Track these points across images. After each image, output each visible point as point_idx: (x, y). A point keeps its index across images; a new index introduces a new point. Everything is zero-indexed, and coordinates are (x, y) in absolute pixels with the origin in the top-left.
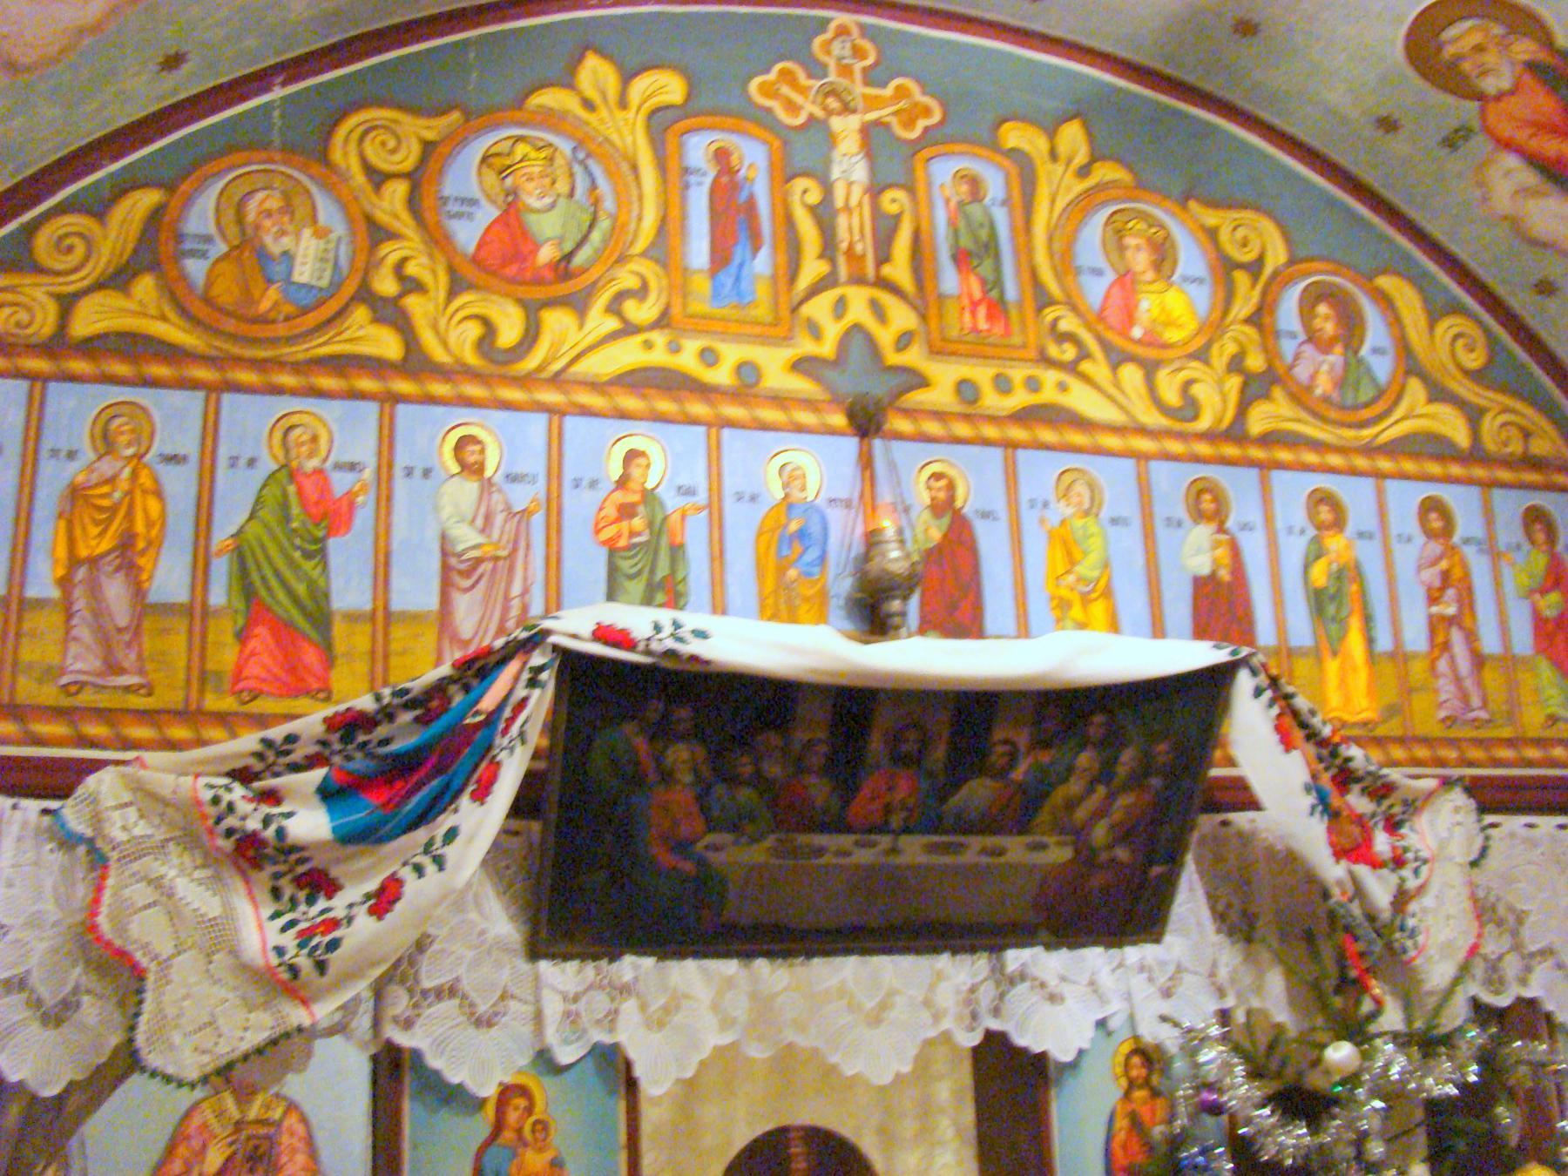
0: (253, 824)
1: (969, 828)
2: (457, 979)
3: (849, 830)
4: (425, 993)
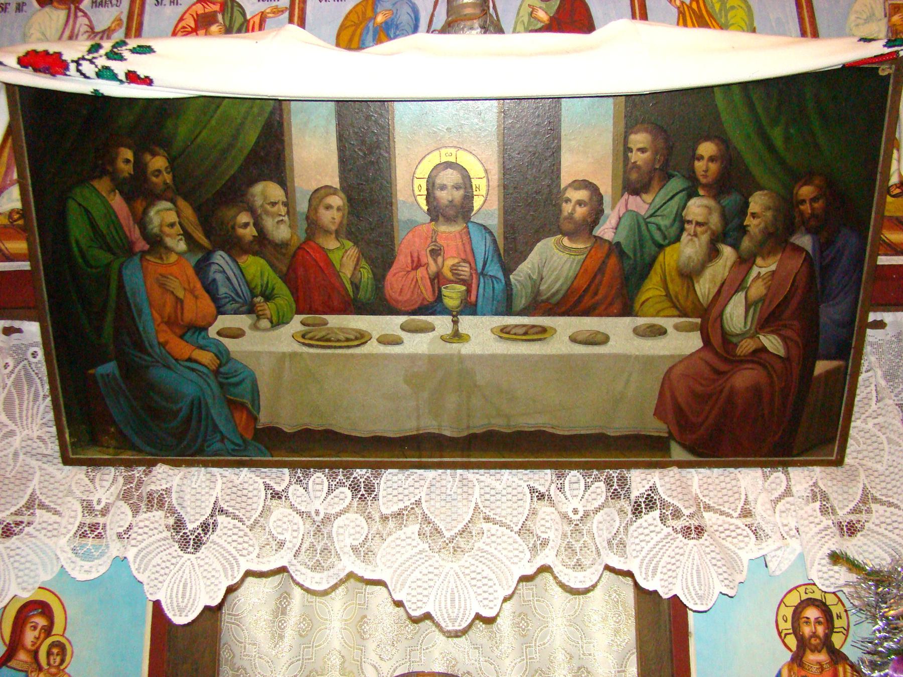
2: (168, 491)
4: (385, 518)
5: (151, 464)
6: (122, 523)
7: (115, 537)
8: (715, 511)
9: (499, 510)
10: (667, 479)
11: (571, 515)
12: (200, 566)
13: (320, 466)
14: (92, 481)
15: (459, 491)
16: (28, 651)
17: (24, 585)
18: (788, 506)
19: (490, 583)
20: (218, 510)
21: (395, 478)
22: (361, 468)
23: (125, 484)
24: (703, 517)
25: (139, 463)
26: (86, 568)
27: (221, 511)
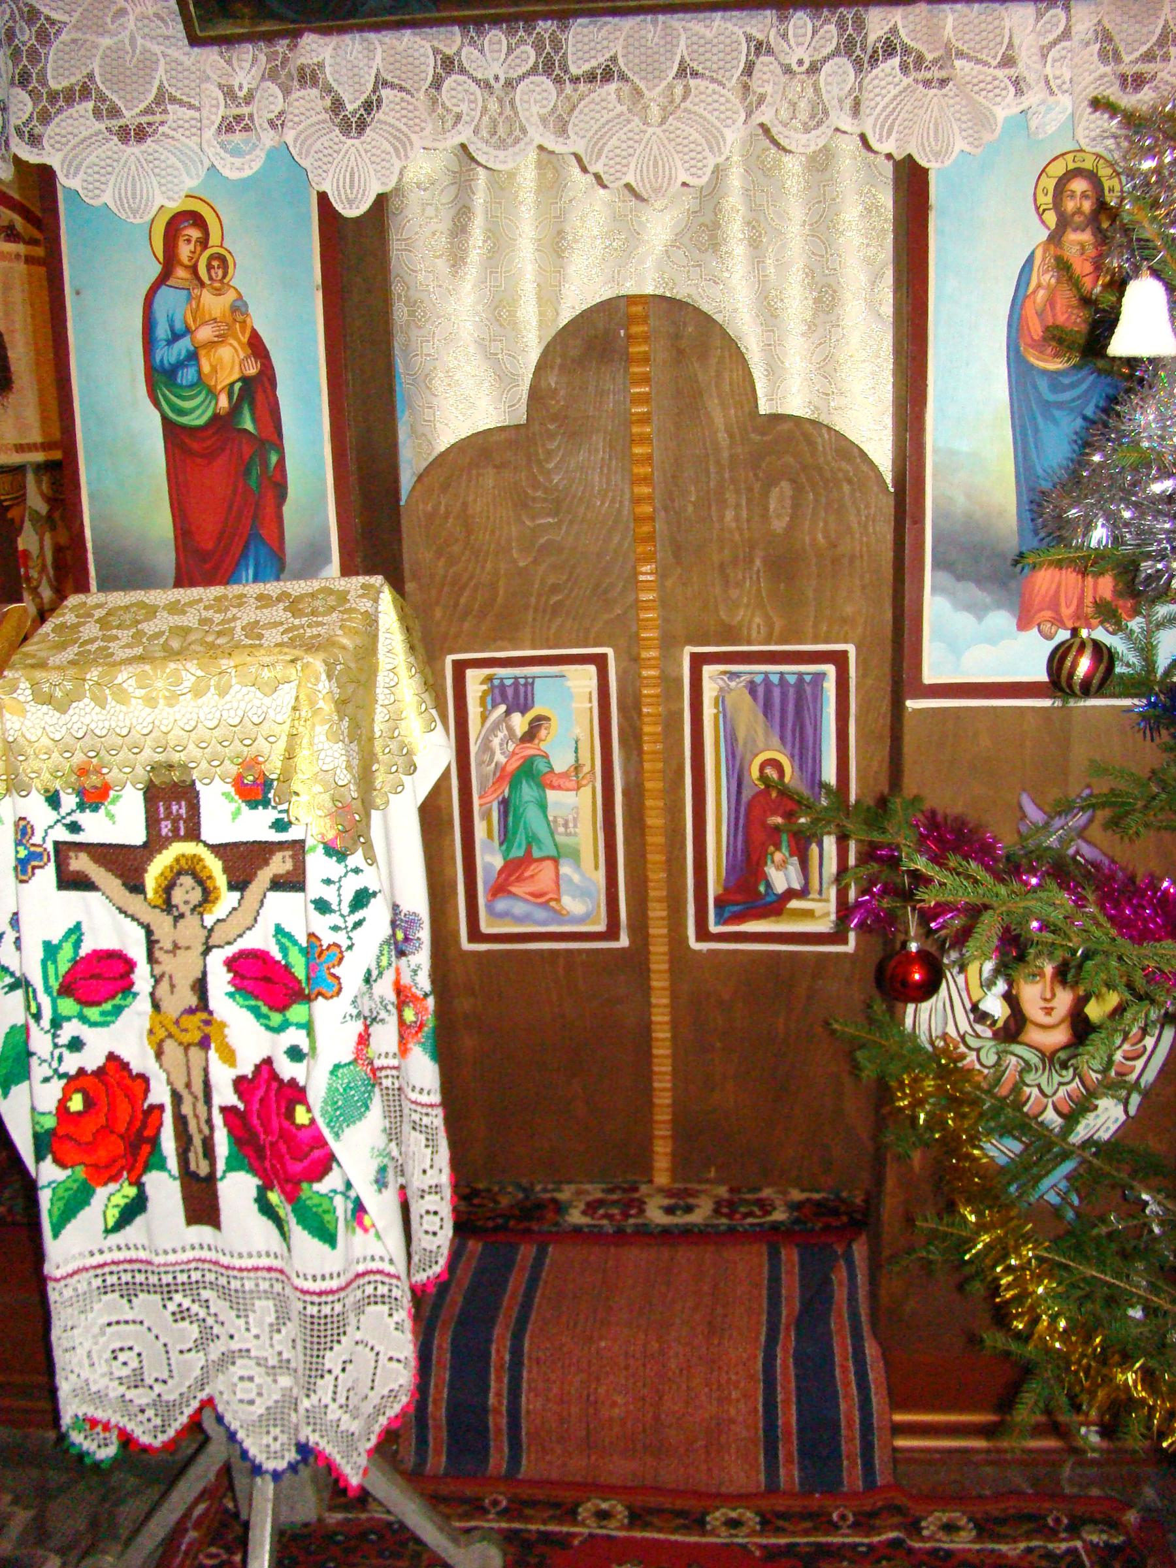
2: (321, 65)
4: (53, 97)
5: (296, 34)
6: (272, 107)
7: (266, 125)
8: (969, 58)
9: (708, 64)
10: (911, 18)
11: (795, 67)
12: (366, 151)
13: (496, 21)
14: (229, 62)
15: (662, 42)
16: (186, 267)
17: (170, 194)
18: (1064, 53)
19: (699, 149)
20: (381, 82)
21: (585, 31)
22: (545, 19)
23: (268, 61)
24: (953, 67)
25: (282, 34)
26: (238, 165)
27: (385, 84)
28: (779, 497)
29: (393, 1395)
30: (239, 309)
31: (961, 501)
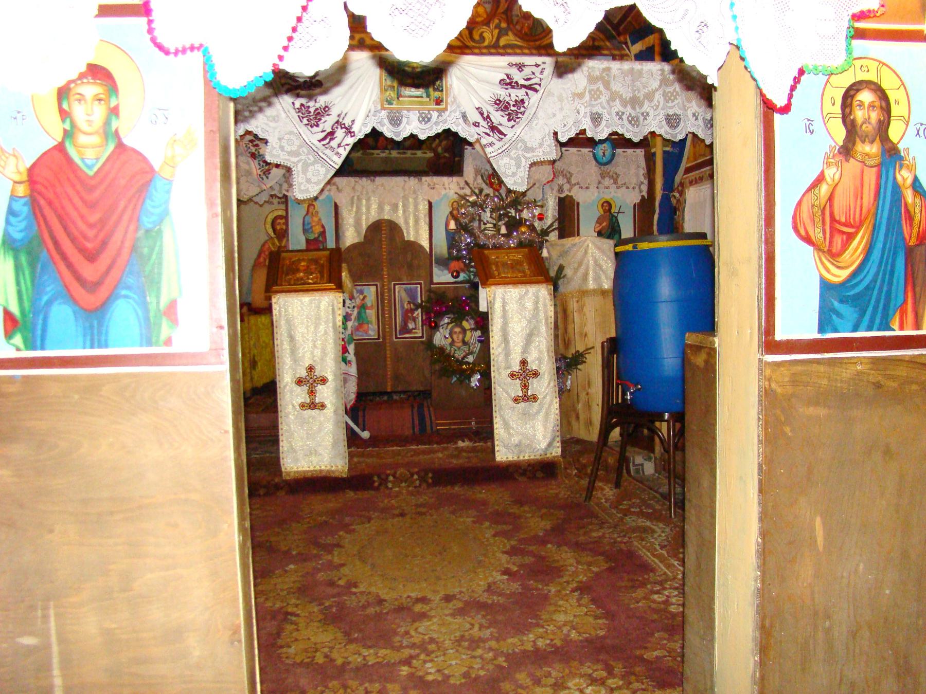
0: (254, 151)
1: (408, 149)
3: (379, 149)
28: (409, 256)
29: (351, 400)
30: (320, 220)
31: (438, 252)
